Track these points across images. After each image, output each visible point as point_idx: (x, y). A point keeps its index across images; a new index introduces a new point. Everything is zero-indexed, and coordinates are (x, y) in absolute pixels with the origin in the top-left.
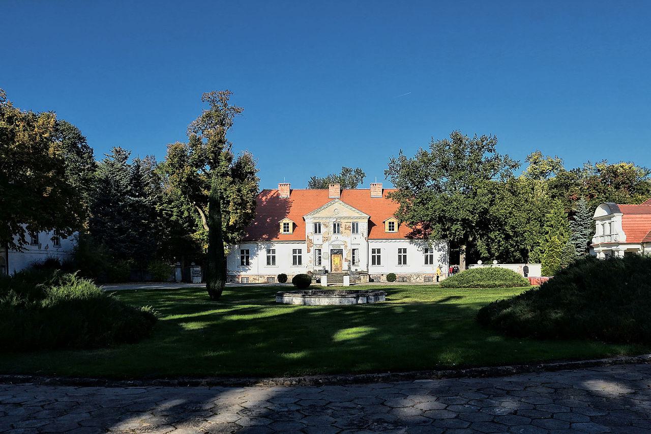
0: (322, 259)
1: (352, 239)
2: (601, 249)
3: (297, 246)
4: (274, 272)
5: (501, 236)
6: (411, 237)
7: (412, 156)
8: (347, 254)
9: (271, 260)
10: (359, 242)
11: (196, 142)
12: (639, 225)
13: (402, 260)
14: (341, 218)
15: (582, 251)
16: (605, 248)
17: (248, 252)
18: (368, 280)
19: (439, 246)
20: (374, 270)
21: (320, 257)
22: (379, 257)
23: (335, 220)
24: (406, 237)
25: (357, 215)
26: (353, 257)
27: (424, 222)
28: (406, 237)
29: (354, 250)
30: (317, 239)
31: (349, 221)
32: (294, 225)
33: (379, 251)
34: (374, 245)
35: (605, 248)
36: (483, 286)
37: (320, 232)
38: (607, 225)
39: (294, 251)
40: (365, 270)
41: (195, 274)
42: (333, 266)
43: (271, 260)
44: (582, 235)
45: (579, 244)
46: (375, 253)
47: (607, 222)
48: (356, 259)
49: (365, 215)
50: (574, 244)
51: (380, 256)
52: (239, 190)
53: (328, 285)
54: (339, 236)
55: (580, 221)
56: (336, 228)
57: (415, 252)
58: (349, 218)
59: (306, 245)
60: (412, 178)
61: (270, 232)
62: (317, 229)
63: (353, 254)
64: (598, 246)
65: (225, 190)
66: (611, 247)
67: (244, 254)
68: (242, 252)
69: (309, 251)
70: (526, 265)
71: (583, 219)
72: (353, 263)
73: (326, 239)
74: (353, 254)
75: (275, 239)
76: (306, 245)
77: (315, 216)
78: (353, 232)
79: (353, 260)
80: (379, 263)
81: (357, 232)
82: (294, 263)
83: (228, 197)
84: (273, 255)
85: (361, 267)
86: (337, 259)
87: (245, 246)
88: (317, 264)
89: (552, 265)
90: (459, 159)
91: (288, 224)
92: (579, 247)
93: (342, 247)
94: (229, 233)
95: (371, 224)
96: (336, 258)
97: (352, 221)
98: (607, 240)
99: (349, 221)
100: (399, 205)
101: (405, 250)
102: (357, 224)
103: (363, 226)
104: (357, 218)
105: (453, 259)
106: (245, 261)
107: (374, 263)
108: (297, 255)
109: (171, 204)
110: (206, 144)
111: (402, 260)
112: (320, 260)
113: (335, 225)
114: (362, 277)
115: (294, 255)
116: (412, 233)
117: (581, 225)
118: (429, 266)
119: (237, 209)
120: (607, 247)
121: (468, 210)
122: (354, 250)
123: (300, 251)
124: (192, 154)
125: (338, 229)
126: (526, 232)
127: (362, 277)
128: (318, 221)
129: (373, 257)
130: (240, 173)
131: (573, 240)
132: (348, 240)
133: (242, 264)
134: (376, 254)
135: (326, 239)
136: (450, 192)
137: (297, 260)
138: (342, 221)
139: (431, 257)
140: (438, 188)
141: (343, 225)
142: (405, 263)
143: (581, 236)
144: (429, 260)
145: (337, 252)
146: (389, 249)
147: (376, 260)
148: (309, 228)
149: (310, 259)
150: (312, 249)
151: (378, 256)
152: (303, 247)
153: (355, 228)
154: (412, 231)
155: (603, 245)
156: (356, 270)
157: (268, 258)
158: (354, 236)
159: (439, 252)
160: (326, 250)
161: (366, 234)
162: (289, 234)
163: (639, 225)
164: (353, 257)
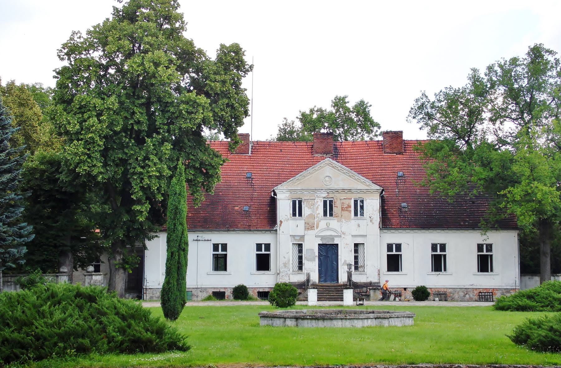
8: (345, 256)
9: (220, 263)
13: (438, 263)
20: (394, 281)
21: (300, 258)
23: (325, 195)
25: (361, 186)
29: (356, 245)
33: (224, 247)
34: (394, 237)
37: (300, 215)
43: (220, 263)
46: (483, 252)
54: (333, 223)
56: (329, 208)
62: (297, 209)
70: (163, 319)
72: (356, 268)
73: (309, 227)
74: (356, 251)
78: (356, 214)
79: (356, 263)
99: (349, 195)
100: (241, 130)
103: (373, 205)
104: (361, 191)
111: (438, 263)
114: (372, 292)
118: (387, 279)
122: (356, 245)
127: (372, 292)
128: (296, 196)
135: (309, 227)
147: (394, 263)
153: (359, 208)
158: (359, 221)
160: (312, 246)
164: (356, 258)
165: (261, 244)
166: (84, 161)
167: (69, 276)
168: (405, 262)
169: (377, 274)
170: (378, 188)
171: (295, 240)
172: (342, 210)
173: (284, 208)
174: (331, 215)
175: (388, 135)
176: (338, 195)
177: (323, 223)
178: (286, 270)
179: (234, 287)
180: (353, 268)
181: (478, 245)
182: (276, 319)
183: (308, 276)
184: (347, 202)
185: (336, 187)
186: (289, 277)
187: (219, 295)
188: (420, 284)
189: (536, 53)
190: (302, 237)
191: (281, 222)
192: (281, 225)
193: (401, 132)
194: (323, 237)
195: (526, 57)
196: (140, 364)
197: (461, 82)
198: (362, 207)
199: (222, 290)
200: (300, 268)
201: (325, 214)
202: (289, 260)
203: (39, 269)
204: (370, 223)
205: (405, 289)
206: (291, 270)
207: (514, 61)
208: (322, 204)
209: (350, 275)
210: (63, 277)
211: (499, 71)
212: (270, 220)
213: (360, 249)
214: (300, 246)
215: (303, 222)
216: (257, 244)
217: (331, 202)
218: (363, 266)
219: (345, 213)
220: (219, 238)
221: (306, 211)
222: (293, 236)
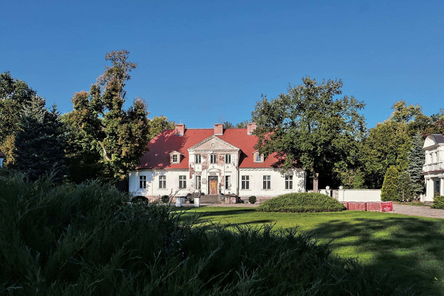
0: (201, 184)
1: (226, 167)
2: (430, 176)
3: (182, 173)
4: (163, 193)
5: (345, 166)
6: (275, 167)
7: (272, 98)
9: (162, 185)
10: (230, 169)
11: (96, 91)
13: (267, 185)
14: (217, 151)
15: (417, 179)
16: (433, 176)
17: (145, 177)
18: (235, 201)
19: (299, 173)
20: (244, 194)
21: (200, 183)
22: (248, 183)
23: (212, 152)
24: (271, 166)
25: (229, 148)
26: (227, 183)
27: (288, 155)
28: (271, 166)
29: (227, 177)
30: (198, 168)
31: (223, 153)
32: (182, 157)
33: (248, 178)
34: (243, 172)
35: (433, 176)
36: (291, 211)
38: (434, 154)
39: (264, 177)
40: (236, 193)
42: (210, 189)
43: (162, 185)
44: (418, 164)
45: (414, 172)
47: (434, 151)
48: (229, 185)
49: (235, 148)
50: (411, 172)
52: (130, 129)
54: (216, 166)
55: (416, 152)
57: (277, 178)
58: (223, 150)
59: (189, 172)
60: (271, 115)
61: (164, 163)
62: (198, 161)
63: (227, 180)
64: (426, 173)
65: (116, 128)
66: (437, 174)
68: (141, 177)
69: (191, 177)
71: (419, 151)
72: (227, 188)
73: (204, 168)
74: (227, 180)
75: (168, 168)
76: (189, 172)
77: (196, 149)
78: (227, 162)
80: (248, 188)
81: (230, 162)
82: (264, 188)
83: (118, 133)
85: (233, 190)
86: (213, 184)
87: (144, 173)
89: (390, 191)
90: (312, 101)
91: (176, 156)
92: (415, 175)
93: (218, 174)
94: (123, 162)
95: (242, 156)
96: (212, 183)
98: (434, 168)
99: (223, 153)
101: (269, 177)
102: (230, 156)
103: (235, 157)
104: (230, 151)
105: (309, 186)
106: (143, 185)
107: (243, 187)
108: (183, 180)
109: (81, 140)
110: (104, 92)
111: (267, 185)
112: (200, 185)
113: (212, 157)
116: (277, 162)
117: (417, 156)
119: (127, 143)
120: (435, 174)
121: (310, 143)
123: (185, 177)
124: (92, 101)
126: (367, 162)
129: (243, 183)
130: (136, 115)
131: (410, 169)
132: (222, 169)
133: (141, 187)
134: (246, 180)
135: (204, 168)
136: (305, 128)
137: (182, 185)
138: (219, 153)
139: (291, 182)
140: (293, 124)
141: (218, 157)
142: (269, 187)
143: (417, 166)
144: (289, 185)
145: (213, 178)
146: (256, 176)
147: (245, 185)
148: (192, 159)
149: (192, 184)
150: (193, 176)
152: (187, 174)
153: (228, 160)
154: (278, 160)
155: (431, 172)
156: (229, 193)
157: (160, 182)
158: (226, 165)
159: (298, 179)
160: (205, 176)
161: (236, 164)
162: (177, 164)
164: (227, 183)
165: (266, 176)
166: (120, 109)
174: (215, 162)
176: (217, 152)
177: (211, 166)
181: (264, 176)
182: (343, 247)
184: (222, 155)
185: (217, 149)
188: (253, 195)
194: (210, 173)
196: (212, 291)
198: (230, 158)
201: (212, 162)
208: (210, 157)
213: (229, 177)
214: (200, 177)
215: (201, 165)
217: (215, 156)
221: (203, 160)
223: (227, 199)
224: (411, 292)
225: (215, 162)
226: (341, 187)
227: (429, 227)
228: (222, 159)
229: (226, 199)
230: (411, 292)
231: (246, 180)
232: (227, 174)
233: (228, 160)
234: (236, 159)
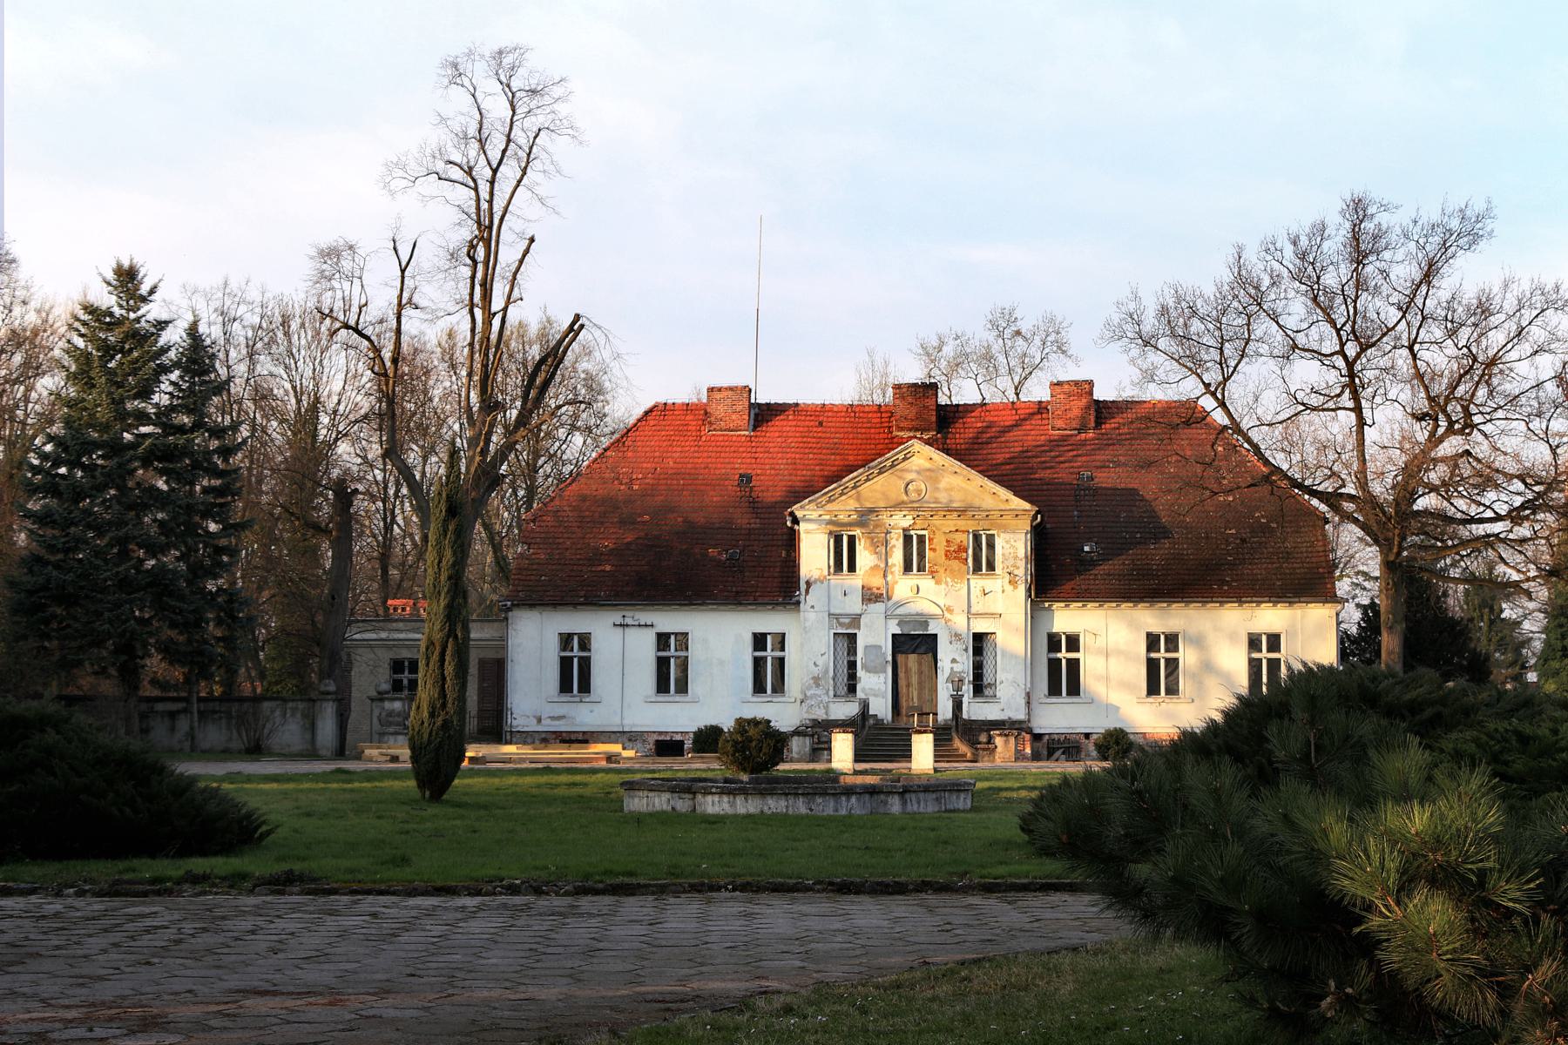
0: (860, 673)
8: (953, 659)
10: (999, 603)
12: (578, 778)
20: (1057, 718)
21: (852, 665)
23: (907, 522)
37: (852, 568)
39: (566, 640)
41: (391, 724)
48: (987, 679)
51: (1176, 660)
53: (936, 770)
54: (926, 583)
62: (843, 557)
67: (1269, 660)
72: (978, 690)
78: (977, 568)
81: (991, 567)
84: (1255, 655)
85: (1007, 701)
88: (843, 690)
97: (971, 526)
103: (1014, 547)
107: (1054, 690)
108: (1264, 655)
112: (852, 676)
113: (908, 539)
115: (1052, 655)
125: (922, 556)
134: (1264, 655)
141: (940, 542)
149: (816, 671)
151: (1269, 660)
158: (977, 583)
160: (876, 635)
163: (578, 778)
167: (339, 701)
168: (749, 640)
169: (1023, 702)
170: (1027, 506)
171: (842, 625)
172: (947, 555)
173: (813, 553)
174: (921, 569)
175: (1058, 389)
177: (903, 587)
178: (818, 692)
179: (695, 729)
180: (967, 689)
183: (865, 705)
184: (959, 537)
186: (827, 708)
187: (668, 747)
189: (1358, 209)
190: (856, 620)
191: (808, 584)
192: (807, 592)
193: (1091, 383)
195: (1340, 219)
197: (1207, 278)
199: (678, 738)
200: (852, 689)
201: (908, 568)
202: (827, 671)
203: (465, 763)
204: (1009, 588)
205: (1087, 736)
206: (831, 693)
207: (1320, 230)
209: (958, 705)
210: (325, 704)
211: (1289, 251)
212: (779, 584)
214: (852, 638)
216: (755, 635)
217: (921, 539)
218: (993, 685)
219: (955, 564)
220: (670, 621)
221: (864, 558)
222: (834, 617)
223: (1006, 742)
224: (1253, 292)
225: (921, 569)
226: (1372, 753)
227: (1383, 655)
228: (956, 553)
229: (999, 741)
230: (1253, 292)
231: (1063, 655)
232: (980, 626)
233: (981, 559)
234: (1021, 553)
